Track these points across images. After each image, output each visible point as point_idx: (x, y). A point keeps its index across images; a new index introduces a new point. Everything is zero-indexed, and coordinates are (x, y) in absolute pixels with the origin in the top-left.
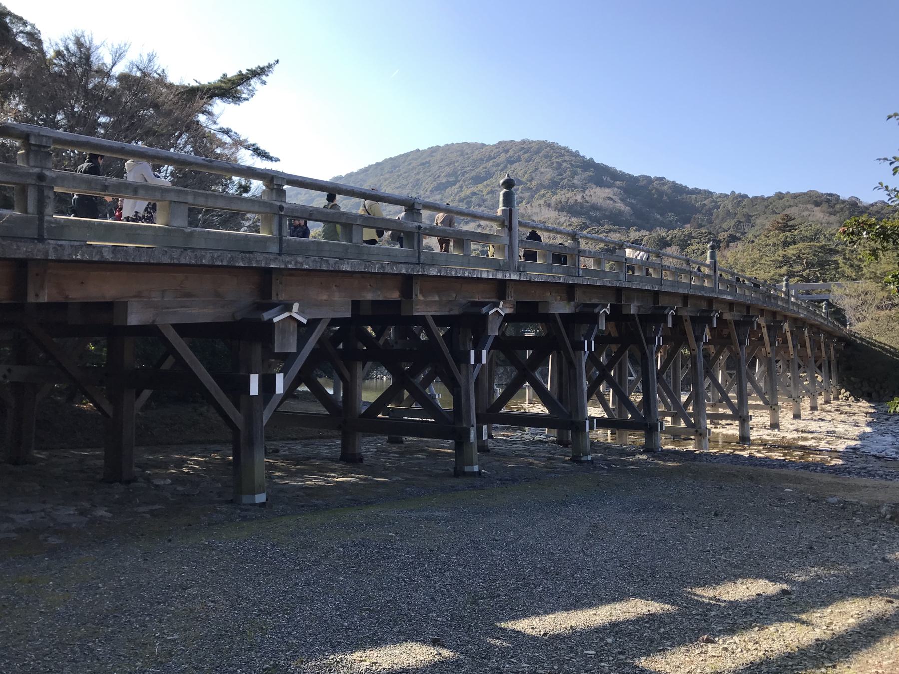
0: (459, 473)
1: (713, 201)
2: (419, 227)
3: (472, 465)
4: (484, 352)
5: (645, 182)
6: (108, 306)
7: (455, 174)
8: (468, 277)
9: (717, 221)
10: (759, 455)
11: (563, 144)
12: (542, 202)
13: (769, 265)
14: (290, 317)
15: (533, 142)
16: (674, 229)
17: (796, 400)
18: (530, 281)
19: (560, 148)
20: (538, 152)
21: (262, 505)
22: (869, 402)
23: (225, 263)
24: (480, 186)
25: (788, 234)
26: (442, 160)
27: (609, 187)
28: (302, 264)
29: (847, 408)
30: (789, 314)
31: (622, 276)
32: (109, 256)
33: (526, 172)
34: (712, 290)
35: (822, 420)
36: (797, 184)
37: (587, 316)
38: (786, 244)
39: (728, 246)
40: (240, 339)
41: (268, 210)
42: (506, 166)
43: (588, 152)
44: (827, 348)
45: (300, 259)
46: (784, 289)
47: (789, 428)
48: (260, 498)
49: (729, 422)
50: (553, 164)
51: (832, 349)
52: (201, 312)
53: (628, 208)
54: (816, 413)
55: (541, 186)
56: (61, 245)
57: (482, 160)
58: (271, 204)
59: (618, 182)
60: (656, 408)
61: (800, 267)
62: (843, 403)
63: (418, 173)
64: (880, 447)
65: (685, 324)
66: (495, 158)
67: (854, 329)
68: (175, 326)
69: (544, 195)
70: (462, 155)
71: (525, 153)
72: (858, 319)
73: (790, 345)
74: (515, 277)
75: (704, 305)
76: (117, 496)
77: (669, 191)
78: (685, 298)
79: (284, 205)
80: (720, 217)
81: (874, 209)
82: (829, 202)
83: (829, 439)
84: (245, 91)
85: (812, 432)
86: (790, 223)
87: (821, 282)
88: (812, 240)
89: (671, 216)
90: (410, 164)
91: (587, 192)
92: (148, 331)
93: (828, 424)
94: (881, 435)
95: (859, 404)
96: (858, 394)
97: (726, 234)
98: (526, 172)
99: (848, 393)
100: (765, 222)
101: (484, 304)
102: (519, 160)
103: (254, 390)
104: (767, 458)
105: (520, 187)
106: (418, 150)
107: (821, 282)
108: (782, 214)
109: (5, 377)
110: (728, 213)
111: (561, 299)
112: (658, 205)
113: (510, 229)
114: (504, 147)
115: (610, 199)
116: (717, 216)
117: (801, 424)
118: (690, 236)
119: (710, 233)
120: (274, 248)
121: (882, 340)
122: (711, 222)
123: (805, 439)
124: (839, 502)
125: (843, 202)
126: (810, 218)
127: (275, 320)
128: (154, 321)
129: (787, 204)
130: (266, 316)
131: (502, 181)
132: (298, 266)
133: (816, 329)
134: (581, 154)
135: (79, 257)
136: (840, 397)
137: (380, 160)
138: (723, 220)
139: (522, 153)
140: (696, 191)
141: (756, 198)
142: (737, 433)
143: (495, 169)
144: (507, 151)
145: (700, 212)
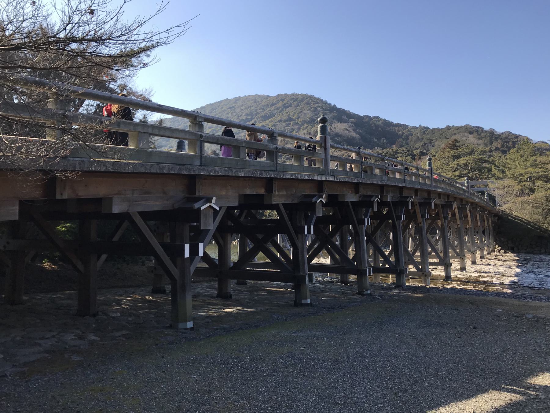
0: (297, 304)
1: (409, 131)
2: (277, 148)
3: (306, 299)
4: (312, 227)
5: (367, 119)
6: (98, 201)
7: (251, 114)
8: (307, 180)
9: (411, 143)
10: (459, 287)
11: (317, 96)
12: (305, 131)
13: (449, 170)
14: (210, 206)
15: (299, 94)
16: (386, 148)
17: (474, 253)
18: (340, 182)
19: (315, 98)
20: (302, 101)
21: (192, 329)
22: (513, 253)
23: (176, 172)
24: (267, 122)
25: (456, 151)
26: (242, 105)
27: (346, 122)
28: (218, 172)
29: (501, 257)
30: (469, 200)
31: (384, 178)
32: (110, 169)
33: (295, 113)
34: (431, 186)
35: (489, 265)
36: (458, 120)
37: (366, 203)
38: (456, 158)
39: (420, 158)
40: (180, 221)
41: (194, 137)
42: (283, 110)
43: (332, 101)
44: (488, 221)
45: (217, 169)
46: (466, 185)
47: (471, 271)
48: (190, 325)
49: (434, 267)
50: (311, 108)
51: (490, 221)
52: (155, 204)
53: (358, 135)
54: (484, 260)
55: (304, 122)
56: (83, 161)
57: (268, 105)
58: (196, 133)
59: (351, 120)
60: (379, 259)
61: (467, 171)
62: (498, 254)
63: (228, 114)
64: (530, 281)
65: (416, 206)
66: (275, 104)
67: (502, 208)
68: (140, 213)
69: (306, 127)
70: (255, 102)
71: (294, 101)
72: (505, 203)
73: (470, 219)
74: (331, 179)
75: (425, 195)
76: (94, 326)
77: (382, 125)
78: (416, 191)
79: (203, 135)
80: (413, 140)
81: (503, 136)
82: (477, 131)
83: (497, 276)
84: (137, 61)
85: (486, 272)
86: (458, 144)
87: (480, 180)
88: (470, 155)
89: (384, 140)
90: (222, 108)
91: (333, 125)
92: (125, 216)
93: (495, 268)
94: (527, 273)
95: (507, 254)
96: (507, 248)
97: (419, 151)
98: (295, 113)
99: (500, 248)
100: (441, 143)
101: (314, 196)
102: (290, 105)
103: (187, 255)
104: (464, 289)
105: (292, 122)
106: (227, 99)
107: (480, 180)
108: (453, 139)
109: (5, 247)
110: (418, 139)
111: (352, 193)
112: (376, 133)
113: (325, 149)
114: (281, 97)
115: (347, 130)
116: (412, 140)
117: (478, 267)
118: (396, 152)
119: (408, 151)
120: (198, 162)
121: (520, 215)
122: (407, 144)
123: (483, 277)
124: (534, 317)
125: (486, 132)
126: (467, 141)
127: (202, 208)
128: (128, 210)
129: (453, 133)
130: (196, 206)
131: (319, 119)
132: (216, 174)
133: (483, 209)
134: (328, 102)
135: (93, 169)
136: (495, 250)
137: (204, 105)
138: (415, 142)
139: (292, 101)
140: (398, 125)
141: (434, 129)
142: (443, 274)
143: (276, 111)
144: (283, 100)
145: (401, 138)
